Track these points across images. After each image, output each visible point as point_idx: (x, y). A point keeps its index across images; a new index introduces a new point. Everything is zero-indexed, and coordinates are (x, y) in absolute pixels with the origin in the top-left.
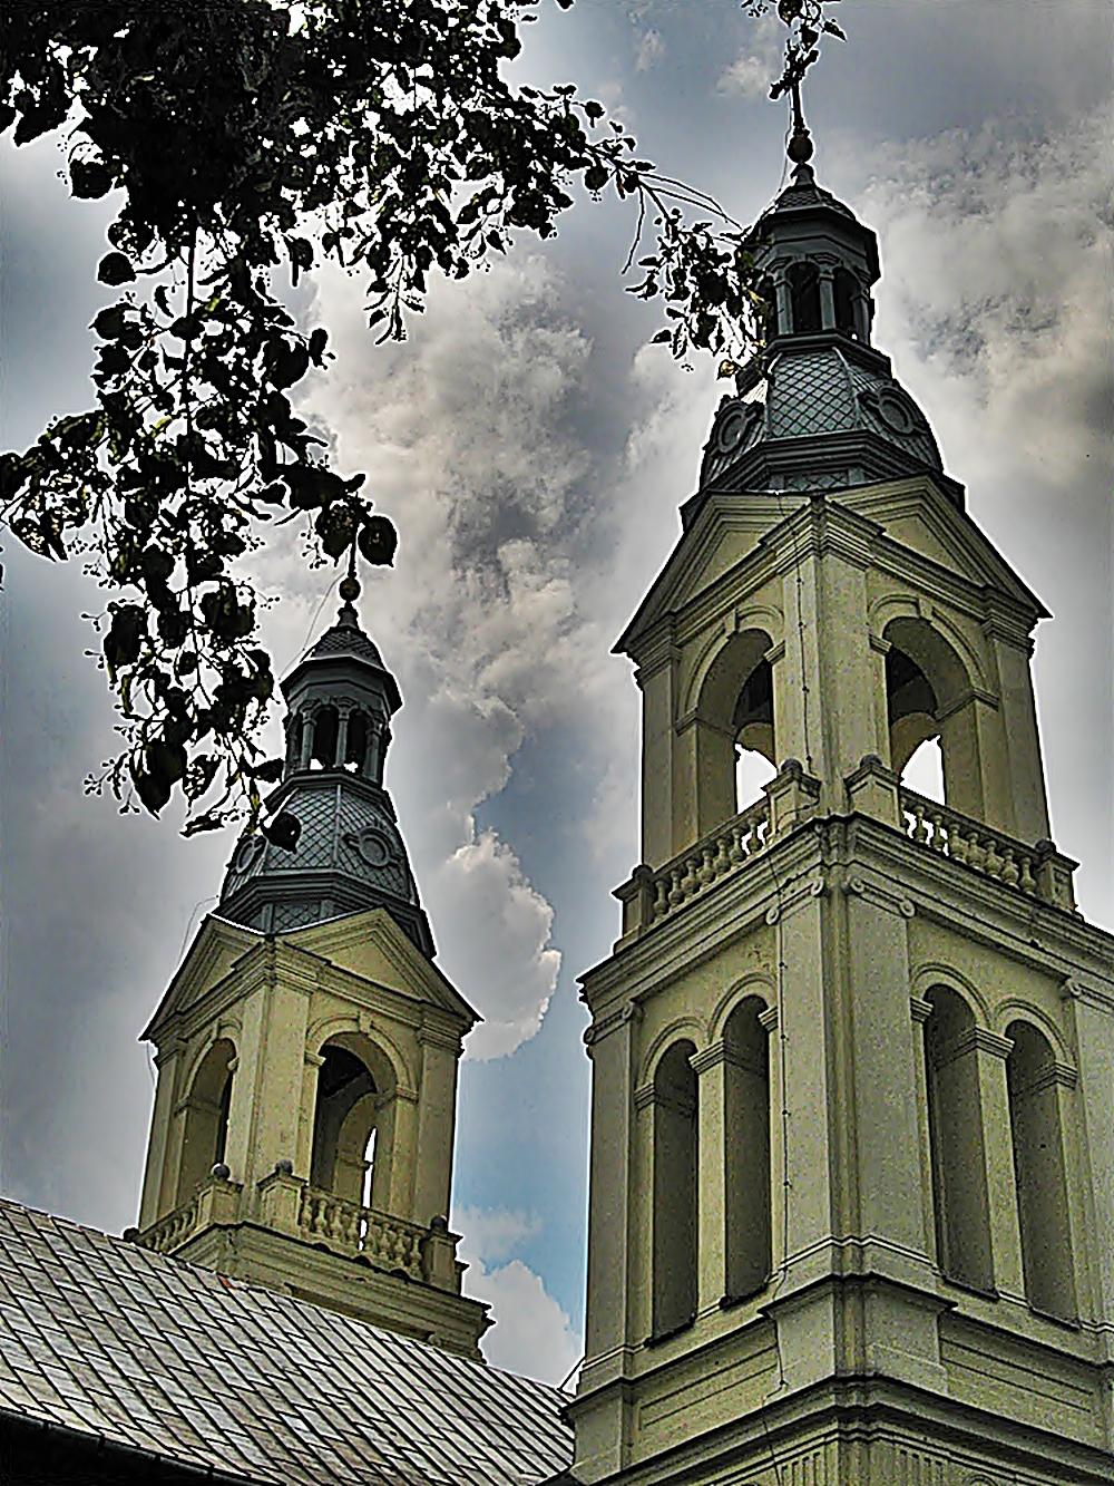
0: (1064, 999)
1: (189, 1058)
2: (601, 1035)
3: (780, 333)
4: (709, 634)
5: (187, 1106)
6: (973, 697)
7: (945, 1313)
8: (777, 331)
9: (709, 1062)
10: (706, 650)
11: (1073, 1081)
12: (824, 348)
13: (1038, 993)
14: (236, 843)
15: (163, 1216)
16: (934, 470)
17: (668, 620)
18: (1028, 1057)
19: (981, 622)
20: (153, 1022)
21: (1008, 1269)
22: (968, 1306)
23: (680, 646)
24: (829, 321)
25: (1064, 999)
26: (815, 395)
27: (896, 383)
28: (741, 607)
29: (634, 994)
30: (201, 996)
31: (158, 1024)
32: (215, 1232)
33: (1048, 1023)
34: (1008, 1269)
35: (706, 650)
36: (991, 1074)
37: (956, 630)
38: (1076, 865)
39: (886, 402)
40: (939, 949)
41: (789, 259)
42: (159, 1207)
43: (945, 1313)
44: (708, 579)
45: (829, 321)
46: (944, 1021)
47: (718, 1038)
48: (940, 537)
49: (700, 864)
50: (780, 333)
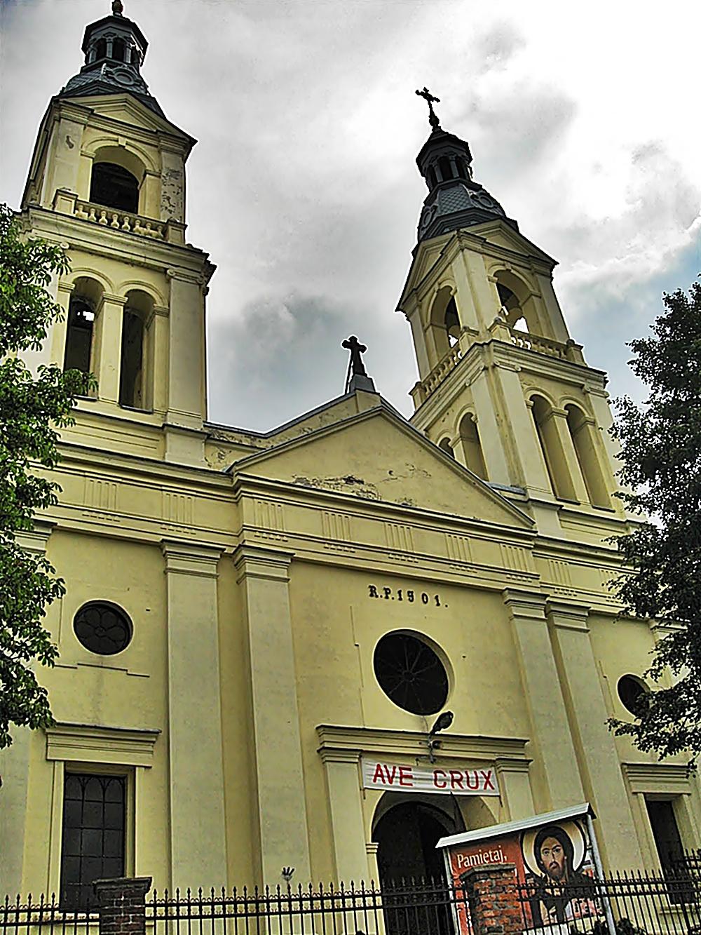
0: (584, 394)
1: (425, 307)
2: (473, 380)
3: (439, 181)
4: (429, 295)
5: (431, 324)
6: (532, 295)
7: (560, 510)
8: (437, 181)
9: (455, 442)
10: (429, 300)
11: (594, 423)
12: (457, 184)
13: (573, 392)
14: (417, 230)
15: (433, 368)
16: (503, 217)
17: (414, 292)
18: (573, 415)
19: (530, 269)
20: (401, 299)
21: (581, 493)
22: (566, 506)
23: (421, 301)
24: (456, 175)
25: (584, 394)
26: (454, 201)
27: (484, 190)
28: (439, 280)
29: (424, 428)
30: (419, 283)
31: (403, 301)
32: (476, 348)
33: (580, 404)
34: (581, 493)
35: (429, 300)
36: (562, 425)
37: (521, 274)
38: (582, 347)
39: (482, 198)
40: (536, 382)
41: (437, 156)
42: (430, 364)
43: (560, 510)
44: (430, 266)
45: (456, 175)
46: (539, 408)
47: (458, 432)
48: (507, 239)
49: (444, 368)
50: (439, 181)
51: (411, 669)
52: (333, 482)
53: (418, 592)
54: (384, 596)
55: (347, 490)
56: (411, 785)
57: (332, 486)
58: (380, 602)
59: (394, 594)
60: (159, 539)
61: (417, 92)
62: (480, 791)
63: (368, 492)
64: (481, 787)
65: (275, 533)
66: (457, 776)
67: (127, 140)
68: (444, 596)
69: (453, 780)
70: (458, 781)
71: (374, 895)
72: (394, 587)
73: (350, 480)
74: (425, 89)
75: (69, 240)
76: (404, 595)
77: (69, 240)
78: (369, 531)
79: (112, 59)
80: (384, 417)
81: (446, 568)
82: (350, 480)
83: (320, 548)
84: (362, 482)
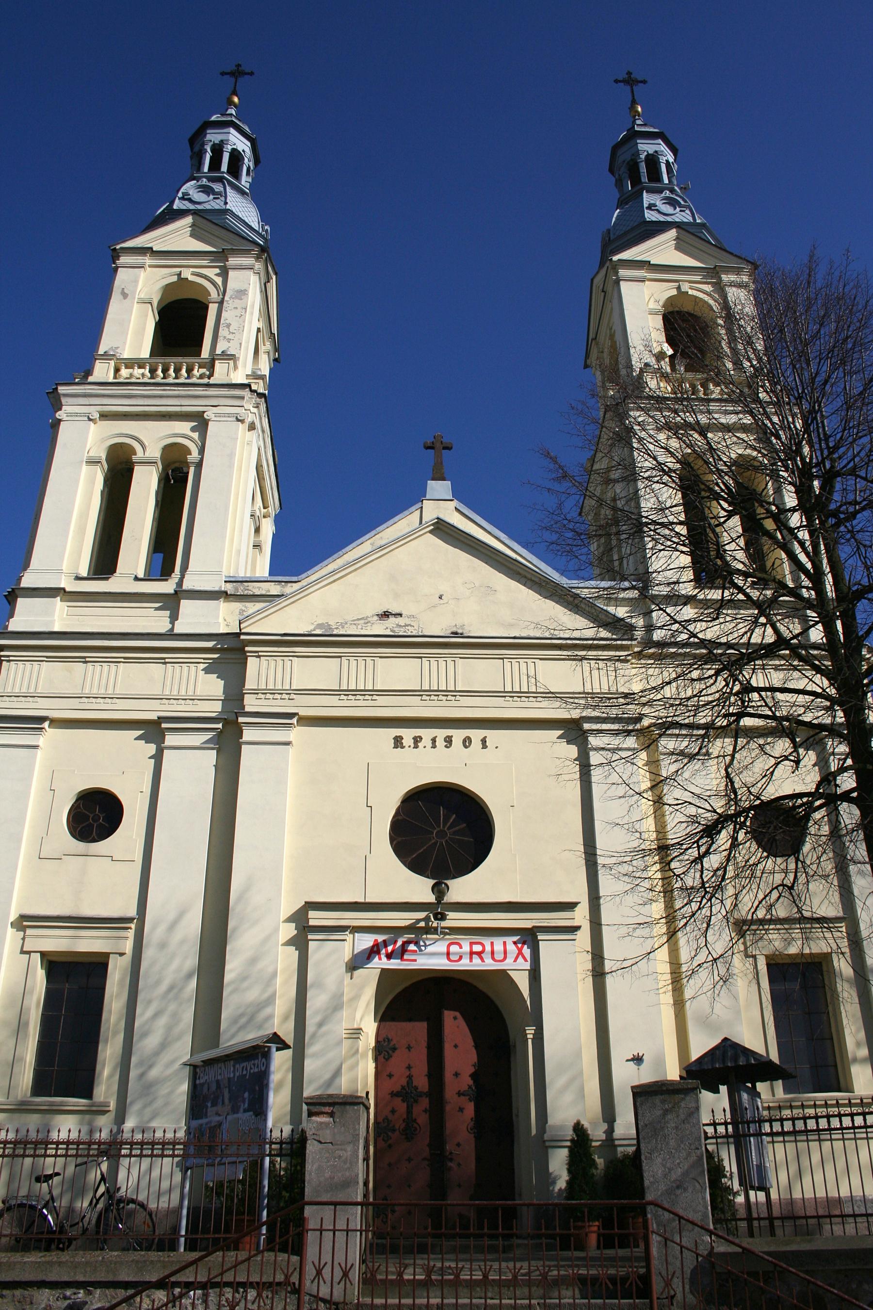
51: (443, 829)
52: (362, 621)
53: (458, 735)
54: (412, 745)
55: (380, 628)
56: (415, 960)
57: (360, 627)
58: (407, 753)
59: (426, 741)
60: (153, 716)
61: (616, 81)
62: (508, 965)
63: (406, 625)
64: (510, 960)
65: (528, 694)
66: (477, 948)
67: (192, 270)
68: (493, 736)
69: (472, 953)
70: (479, 954)
71: (726, 1124)
72: (427, 734)
73: (386, 615)
74: (629, 73)
75: (99, 408)
76: (440, 742)
77: (99, 408)
78: (398, 671)
79: (645, 125)
80: (441, 530)
81: (500, 701)
82: (386, 615)
83: (334, 700)
84: (401, 615)
